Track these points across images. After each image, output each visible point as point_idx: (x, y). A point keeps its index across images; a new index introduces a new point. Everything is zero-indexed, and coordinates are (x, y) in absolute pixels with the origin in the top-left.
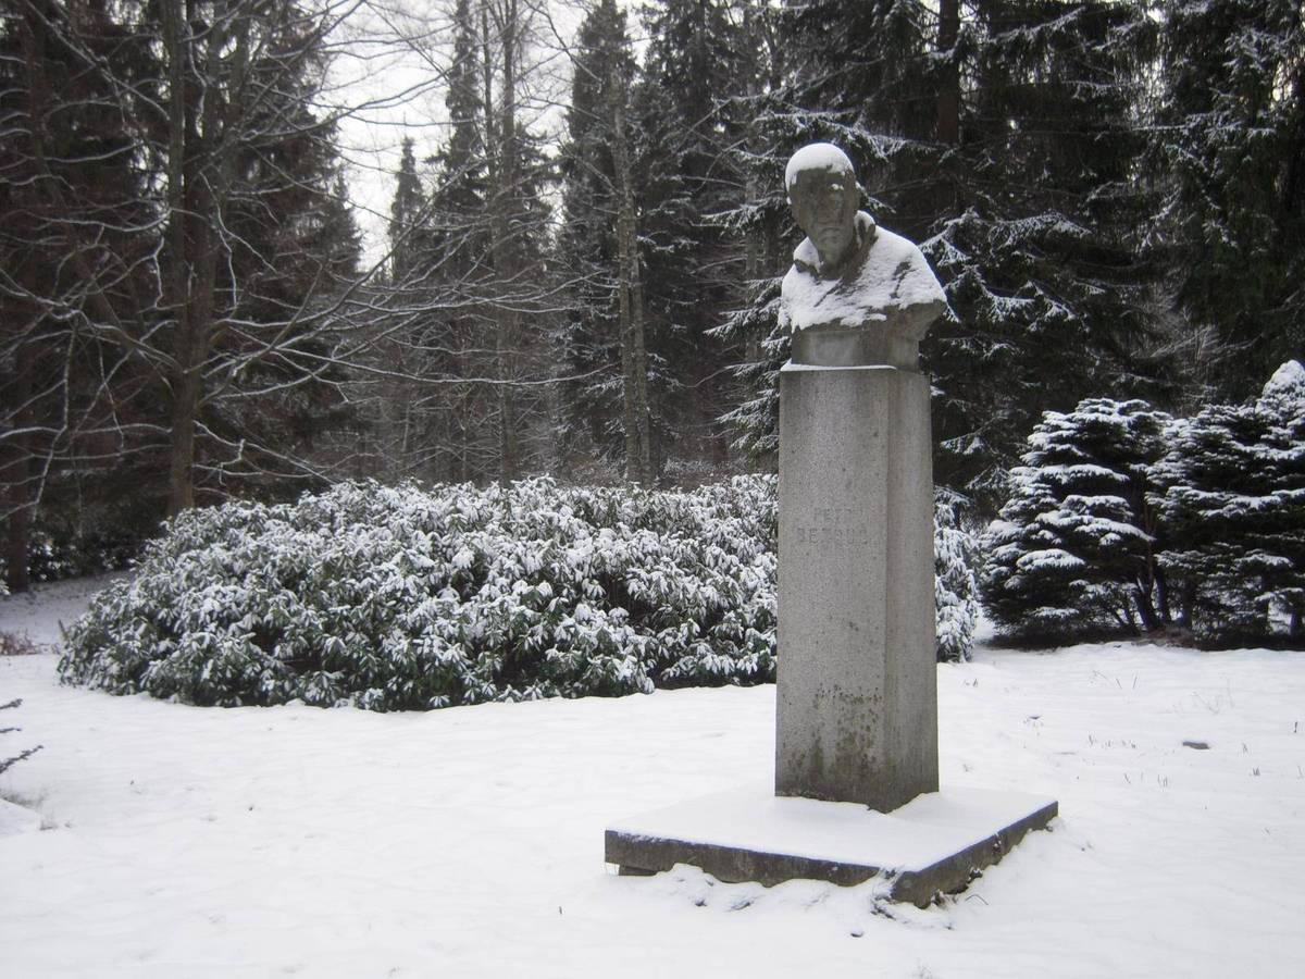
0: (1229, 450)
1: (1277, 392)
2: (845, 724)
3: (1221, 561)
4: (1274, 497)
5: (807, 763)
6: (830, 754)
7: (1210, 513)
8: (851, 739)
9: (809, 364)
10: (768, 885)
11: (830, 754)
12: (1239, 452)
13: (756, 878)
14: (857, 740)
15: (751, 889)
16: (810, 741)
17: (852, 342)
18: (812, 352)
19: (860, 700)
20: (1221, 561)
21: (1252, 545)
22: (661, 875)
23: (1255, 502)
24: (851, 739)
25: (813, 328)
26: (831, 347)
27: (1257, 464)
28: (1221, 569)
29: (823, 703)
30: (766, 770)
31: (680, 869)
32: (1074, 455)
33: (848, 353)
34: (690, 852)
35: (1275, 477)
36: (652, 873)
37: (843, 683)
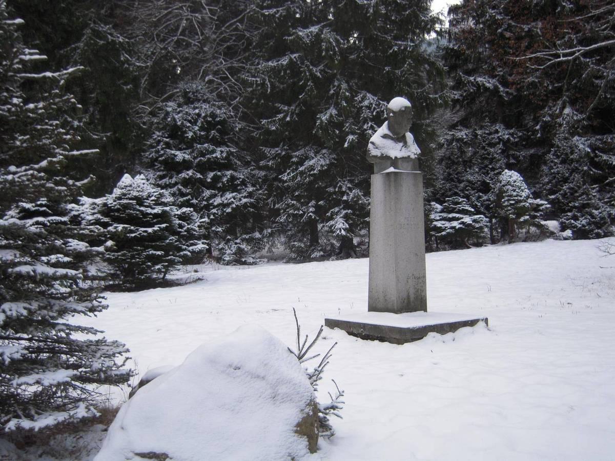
0: (135, 209)
1: (127, 186)
2: (416, 286)
3: (137, 254)
4: (156, 228)
5: (406, 301)
6: (412, 296)
7: (133, 235)
8: (418, 291)
9: (398, 169)
10: (454, 332)
11: (412, 296)
12: (139, 210)
13: (450, 331)
15: (450, 335)
17: (411, 163)
18: (400, 166)
19: (419, 278)
20: (137, 254)
21: (146, 247)
22: (425, 338)
23: (150, 230)
24: (418, 291)
25: (403, 158)
26: (405, 165)
27: (146, 215)
28: (137, 258)
29: (410, 281)
30: (367, 309)
31: (431, 334)
32: (48, 212)
33: (409, 168)
34: (432, 328)
35: (152, 220)
36: (422, 338)
37: (415, 273)
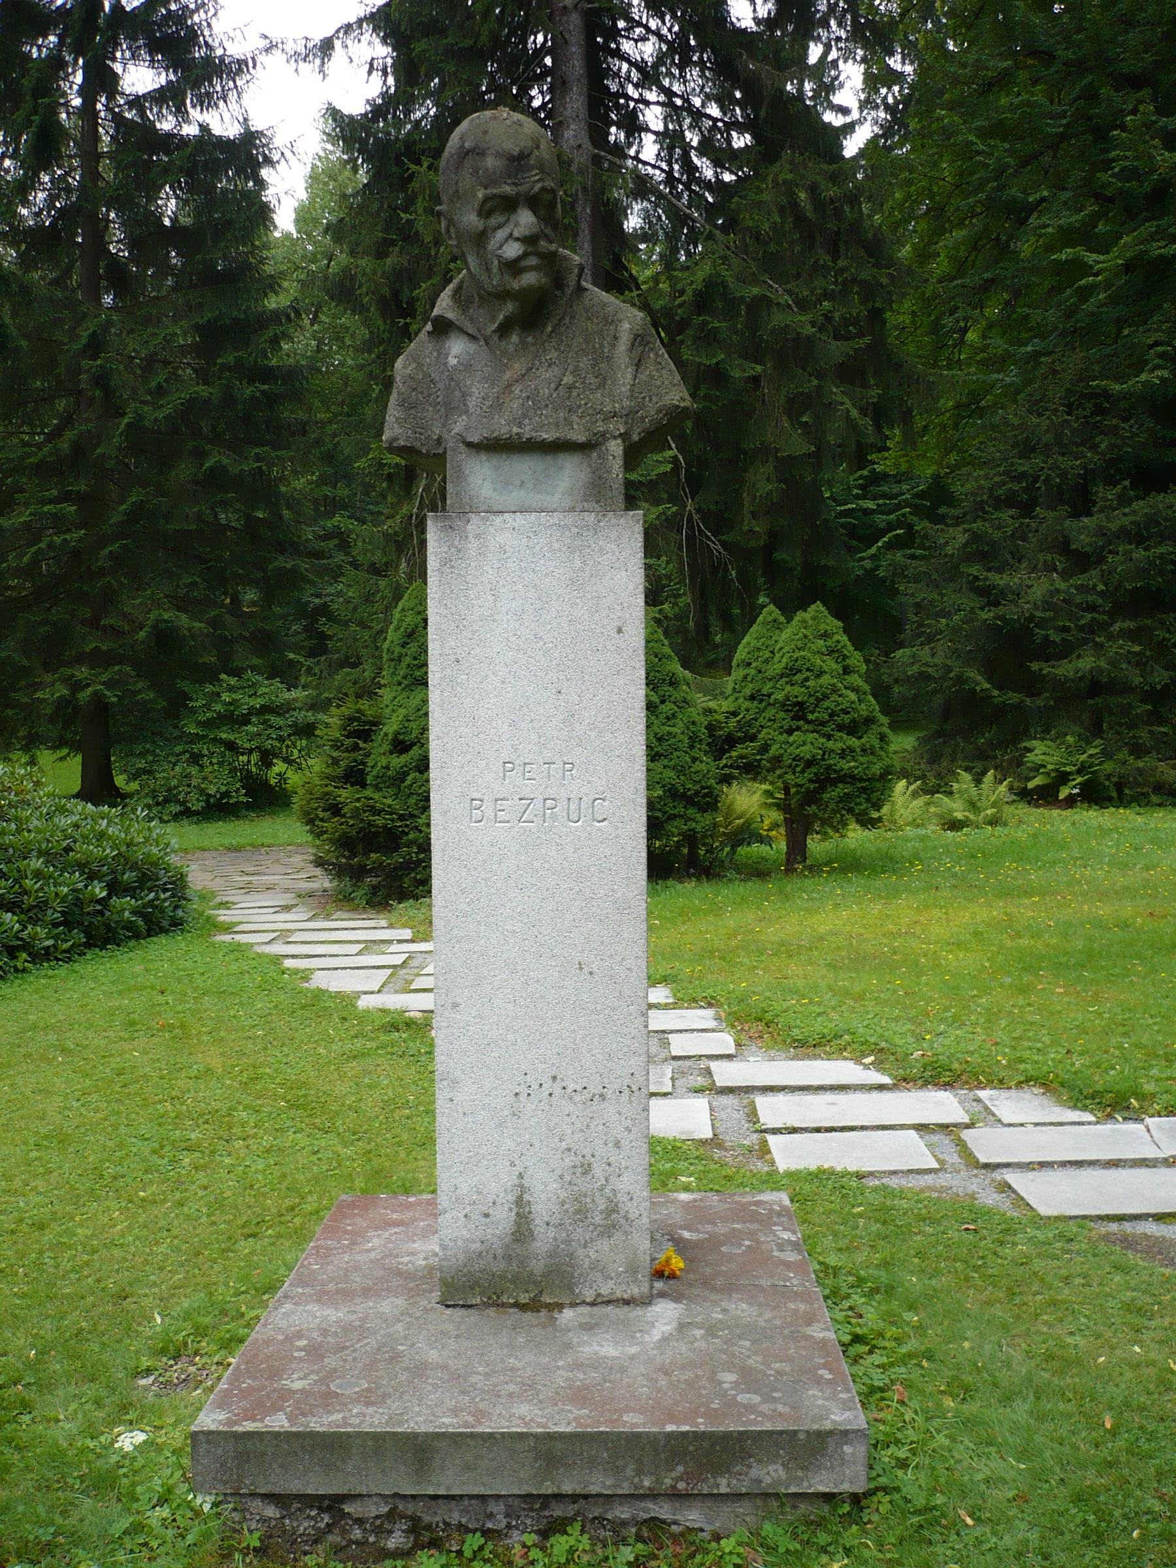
14: (598, 1170)
16: (508, 1178)
24: (587, 1169)
